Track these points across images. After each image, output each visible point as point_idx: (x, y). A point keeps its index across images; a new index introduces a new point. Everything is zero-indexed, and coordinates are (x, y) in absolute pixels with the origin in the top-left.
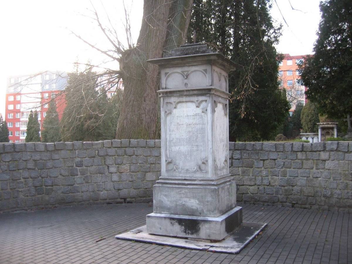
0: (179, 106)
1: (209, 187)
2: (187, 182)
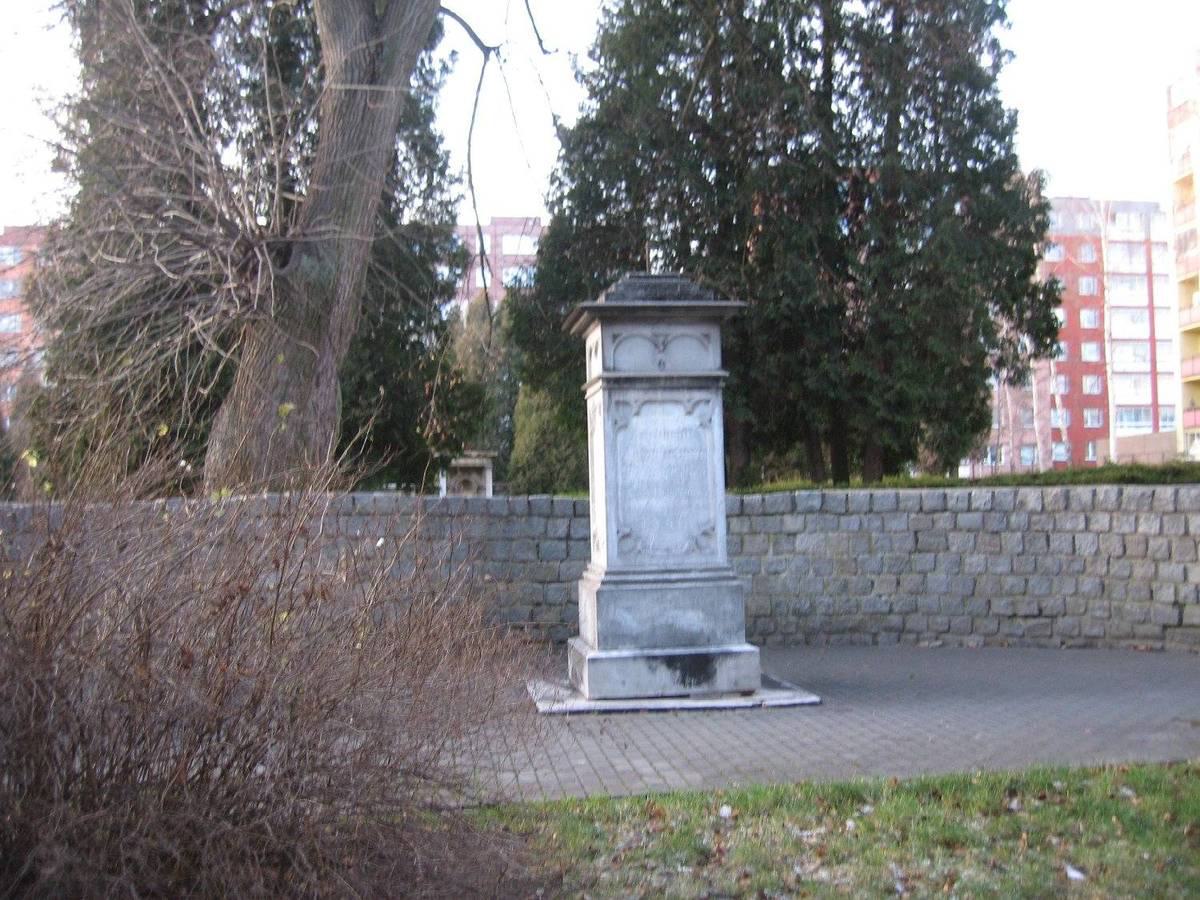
0: (645, 409)
1: (725, 583)
2: (674, 576)
